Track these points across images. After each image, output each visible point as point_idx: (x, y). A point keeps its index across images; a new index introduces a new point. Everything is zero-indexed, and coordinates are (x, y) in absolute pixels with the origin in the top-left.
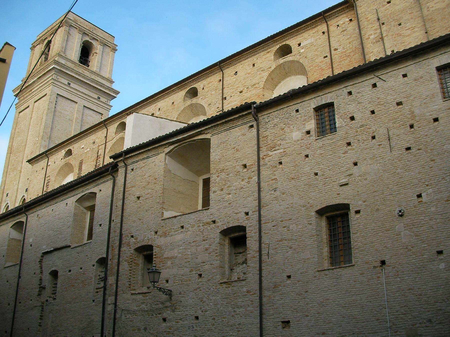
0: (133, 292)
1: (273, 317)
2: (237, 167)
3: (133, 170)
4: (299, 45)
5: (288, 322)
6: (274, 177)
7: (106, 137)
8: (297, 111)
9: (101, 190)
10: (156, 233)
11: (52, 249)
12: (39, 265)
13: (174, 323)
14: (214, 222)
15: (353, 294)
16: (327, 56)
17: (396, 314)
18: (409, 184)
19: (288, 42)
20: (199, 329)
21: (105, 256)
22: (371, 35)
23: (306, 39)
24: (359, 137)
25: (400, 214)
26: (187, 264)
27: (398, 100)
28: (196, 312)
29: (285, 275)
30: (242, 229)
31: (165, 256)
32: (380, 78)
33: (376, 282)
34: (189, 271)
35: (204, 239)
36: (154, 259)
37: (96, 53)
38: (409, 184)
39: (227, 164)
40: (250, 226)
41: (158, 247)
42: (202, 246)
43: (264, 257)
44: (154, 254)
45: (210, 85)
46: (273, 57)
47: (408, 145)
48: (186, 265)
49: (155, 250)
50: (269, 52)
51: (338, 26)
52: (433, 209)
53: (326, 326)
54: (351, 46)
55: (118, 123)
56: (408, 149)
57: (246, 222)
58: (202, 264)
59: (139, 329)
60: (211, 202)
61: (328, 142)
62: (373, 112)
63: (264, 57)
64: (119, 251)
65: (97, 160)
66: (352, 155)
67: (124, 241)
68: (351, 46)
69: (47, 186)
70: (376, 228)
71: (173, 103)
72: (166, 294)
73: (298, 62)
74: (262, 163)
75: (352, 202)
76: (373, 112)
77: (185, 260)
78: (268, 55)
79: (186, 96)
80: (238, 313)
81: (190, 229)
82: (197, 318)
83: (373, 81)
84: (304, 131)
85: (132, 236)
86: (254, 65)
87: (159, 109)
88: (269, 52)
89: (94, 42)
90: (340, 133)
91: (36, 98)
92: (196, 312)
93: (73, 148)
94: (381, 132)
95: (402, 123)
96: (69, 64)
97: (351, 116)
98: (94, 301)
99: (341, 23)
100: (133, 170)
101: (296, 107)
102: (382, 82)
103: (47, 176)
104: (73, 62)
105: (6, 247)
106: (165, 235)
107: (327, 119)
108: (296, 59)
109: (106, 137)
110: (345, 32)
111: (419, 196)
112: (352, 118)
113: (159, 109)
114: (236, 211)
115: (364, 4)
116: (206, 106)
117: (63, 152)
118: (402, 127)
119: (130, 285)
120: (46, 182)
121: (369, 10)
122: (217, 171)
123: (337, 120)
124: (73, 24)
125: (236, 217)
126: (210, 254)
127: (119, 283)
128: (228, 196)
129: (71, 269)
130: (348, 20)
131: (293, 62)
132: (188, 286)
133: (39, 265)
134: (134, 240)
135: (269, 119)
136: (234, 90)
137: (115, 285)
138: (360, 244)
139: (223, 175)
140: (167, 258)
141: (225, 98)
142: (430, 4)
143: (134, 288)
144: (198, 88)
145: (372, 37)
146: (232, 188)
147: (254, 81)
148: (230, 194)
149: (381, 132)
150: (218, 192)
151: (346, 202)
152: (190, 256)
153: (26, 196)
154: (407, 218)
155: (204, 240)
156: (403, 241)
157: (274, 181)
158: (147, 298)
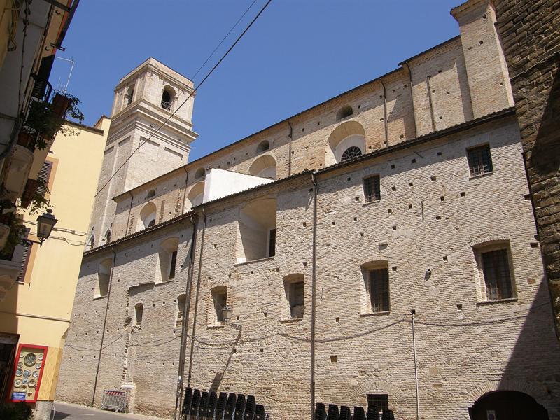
0: (209, 326)
2: (299, 224)
4: (359, 107)
5: (336, 357)
6: (327, 235)
8: (349, 179)
10: (230, 276)
14: (278, 270)
19: (349, 104)
21: (185, 293)
24: (399, 205)
27: (433, 175)
29: (334, 317)
30: (301, 277)
31: (237, 296)
39: (290, 221)
40: (307, 275)
41: (231, 288)
42: (268, 290)
47: (439, 214)
49: (229, 290)
52: (456, 269)
56: (439, 218)
59: (213, 359)
64: (198, 290)
73: (358, 123)
76: (411, 184)
79: (259, 148)
82: (262, 350)
84: (354, 197)
85: (210, 278)
89: (176, 89)
91: (121, 139)
94: (416, 202)
96: (152, 109)
100: (211, 220)
101: (349, 175)
105: (53, 233)
107: (373, 184)
111: (445, 258)
112: (394, 189)
114: (296, 262)
116: (276, 158)
117: (147, 192)
120: (130, 219)
124: (155, 70)
125: (296, 267)
127: (197, 317)
129: (156, 303)
130: (403, 85)
135: (326, 185)
139: (287, 231)
140: (238, 298)
141: (293, 153)
142: (477, 76)
145: (423, 103)
147: (319, 139)
149: (416, 202)
151: (385, 259)
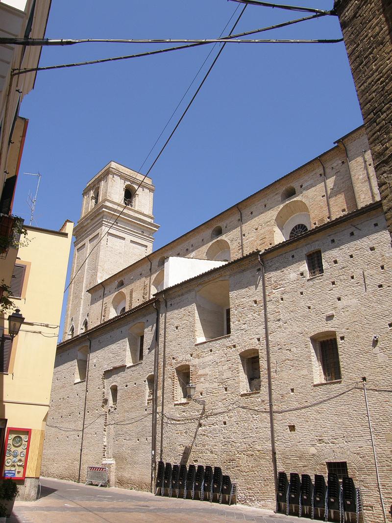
0: (176, 402)
1: (281, 422)
3: (171, 305)
4: (301, 186)
6: (277, 311)
7: (150, 269)
9: (148, 321)
11: (112, 368)
12: (102, 382)
13: (208, 427)
14: (234, 346)
15: (341, 404)
16: (324, 196)
17: (377, 421)
18: (382, 315)
20: (226, 432)
22: (360, 175)
23: (306, 181)
24: (342, 277)
25: (376, 339)
26: (216, 380)
28: (224, 418)
29: (289, 388)
30: (256, 351)
31: (199, 373)
32: (356, 228)
33: (359, 395)
34: (217, 385)
35: (228, 360)
36: (191, 376)
37: (138, 195)
38: (382, 315)
43: (272, 374)
44: (191, 372)
45: (231, 224)
46: (280, 198)
48: (214, 380)
49: (192, 368)
50: (277, 194)
51: (332, 168)
53: (323, 430)
54: (344, 186)
55: (159, 258)
56: (380, 286)
57: (259, 346)
58: (227, 380)
60: (231, 330)
61: (317, 281)
62: (351, 256)
63: (273, 198)
64: (164, 369)
65: (145, 288)
66: (336, 292)
67: (167, 362)
68: (344, 186)
69: (105, 311)
70: (357, 351)
71: (203, 240)
72: (201, 405)
73: (301, 201)
74: (268, 299)
75: (337, 330)
76: (351, 256)
77: (215, 377)
78: (276, 197)
79: (213, 234)
80: (255, 418)
81: (217, 351)
82: (225, 423)
83: (350, 231)
84: (299, 273)
85: (174, 358)
86: (265, 206)
87: (192, 245)
88: (277, 194)
90: (326, 274)
91: (91, 237)
92: (224, 418)
93: (124, 279)
94: (358, 273)
95: (374, 264)
97: (334, 260)
98: (146, 410)
99: (335, 165)
100: (171, 305)
102: (358, 231)
103: (104, 303)
104: (119, 205)
106: (198, 357)
108: (299, 200)
109: (150, 269)
110: (339, 173)
112: (336, 262)
113: (192, 245)
115: (353, 148)
116: (229, 242)
117: (116, 283)
118: (375, 268)
119: (173, 397)
120: (104, 308)
121: (357, 153)
122: (235, 306)
123: (323, 264)
126: (232, 371)
128: (244, 325)
129: (128, 384)
130: (340, 162)
131: (297, 201)
132: (217, 397)
133: (102, 382)
134: (175, 361)
135: (272, 263)
136: (250, 228)
137: (161, 397)
138: (345, 364)
139: (240, 309)
141: (244, 235)
143: (176, 399)
144: (222, 227)
146: (247, 319)
148: (245, 324)
149: (358, 273)
150: (237, 322)
151: (333, 329)
152: (218, 373)
153: (88, 319)
154: (381, 343)
155: (228, 361)
156: (380, 361)
157: (278, 314)
158: (187, 407)
